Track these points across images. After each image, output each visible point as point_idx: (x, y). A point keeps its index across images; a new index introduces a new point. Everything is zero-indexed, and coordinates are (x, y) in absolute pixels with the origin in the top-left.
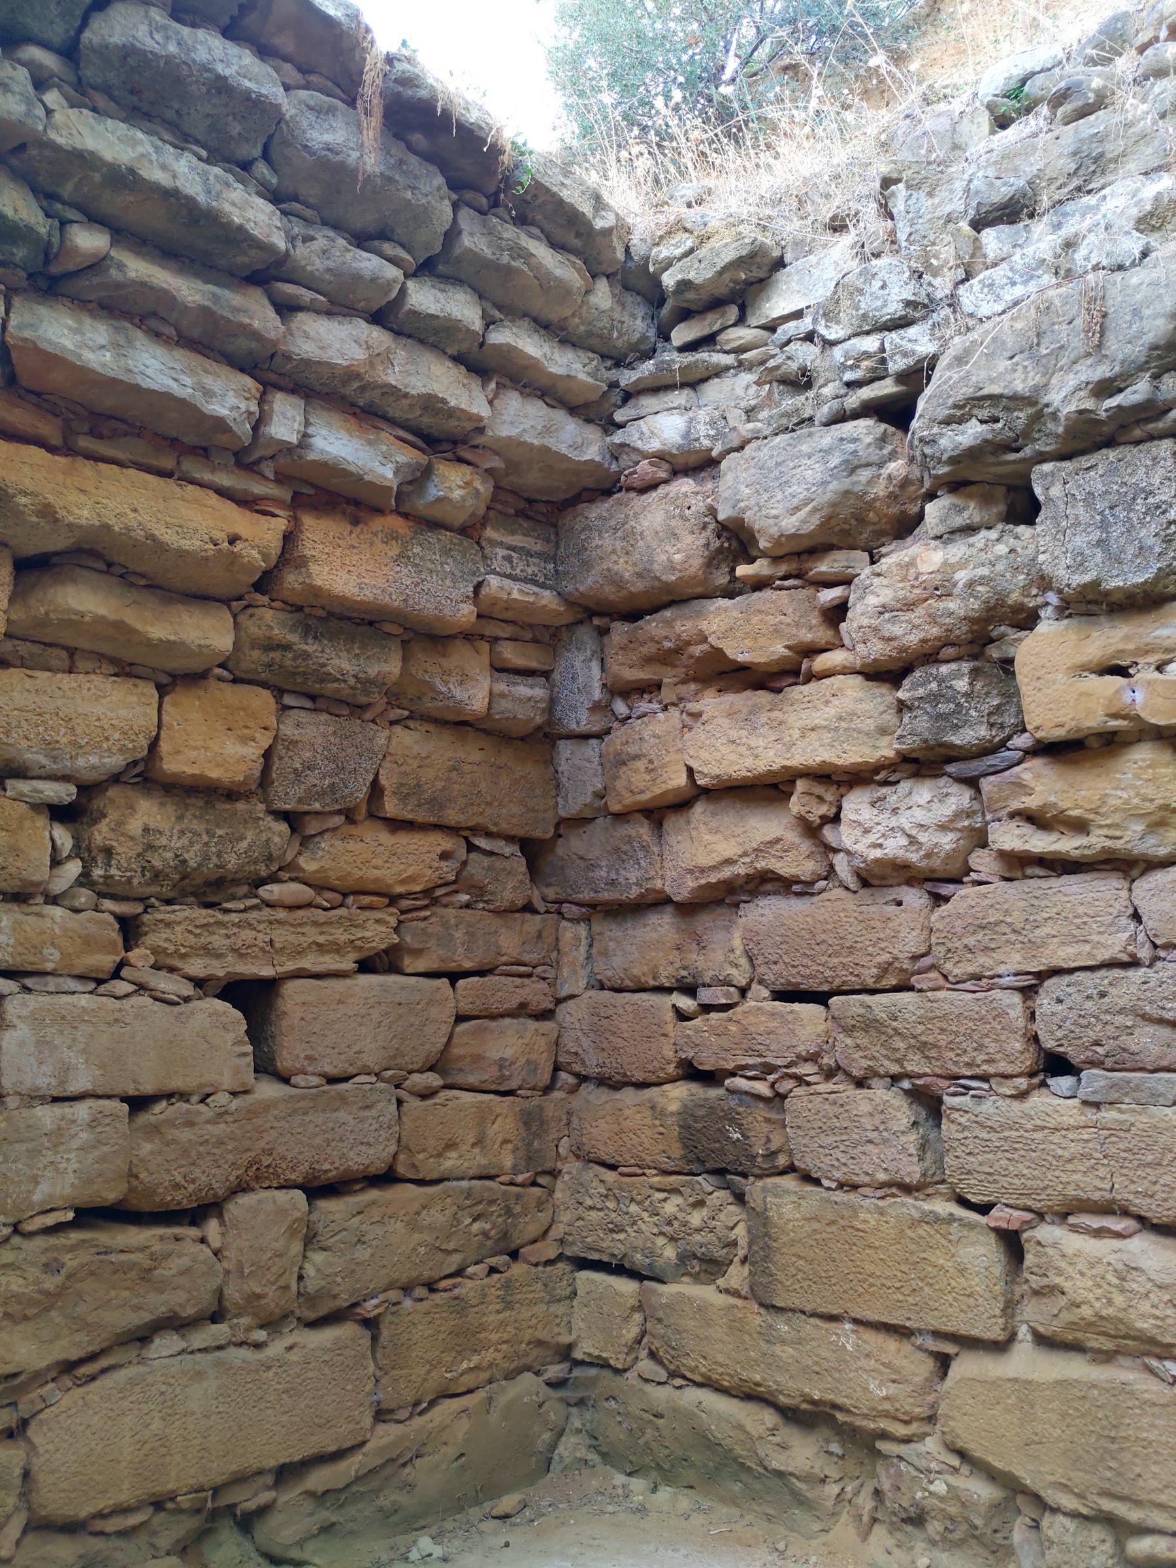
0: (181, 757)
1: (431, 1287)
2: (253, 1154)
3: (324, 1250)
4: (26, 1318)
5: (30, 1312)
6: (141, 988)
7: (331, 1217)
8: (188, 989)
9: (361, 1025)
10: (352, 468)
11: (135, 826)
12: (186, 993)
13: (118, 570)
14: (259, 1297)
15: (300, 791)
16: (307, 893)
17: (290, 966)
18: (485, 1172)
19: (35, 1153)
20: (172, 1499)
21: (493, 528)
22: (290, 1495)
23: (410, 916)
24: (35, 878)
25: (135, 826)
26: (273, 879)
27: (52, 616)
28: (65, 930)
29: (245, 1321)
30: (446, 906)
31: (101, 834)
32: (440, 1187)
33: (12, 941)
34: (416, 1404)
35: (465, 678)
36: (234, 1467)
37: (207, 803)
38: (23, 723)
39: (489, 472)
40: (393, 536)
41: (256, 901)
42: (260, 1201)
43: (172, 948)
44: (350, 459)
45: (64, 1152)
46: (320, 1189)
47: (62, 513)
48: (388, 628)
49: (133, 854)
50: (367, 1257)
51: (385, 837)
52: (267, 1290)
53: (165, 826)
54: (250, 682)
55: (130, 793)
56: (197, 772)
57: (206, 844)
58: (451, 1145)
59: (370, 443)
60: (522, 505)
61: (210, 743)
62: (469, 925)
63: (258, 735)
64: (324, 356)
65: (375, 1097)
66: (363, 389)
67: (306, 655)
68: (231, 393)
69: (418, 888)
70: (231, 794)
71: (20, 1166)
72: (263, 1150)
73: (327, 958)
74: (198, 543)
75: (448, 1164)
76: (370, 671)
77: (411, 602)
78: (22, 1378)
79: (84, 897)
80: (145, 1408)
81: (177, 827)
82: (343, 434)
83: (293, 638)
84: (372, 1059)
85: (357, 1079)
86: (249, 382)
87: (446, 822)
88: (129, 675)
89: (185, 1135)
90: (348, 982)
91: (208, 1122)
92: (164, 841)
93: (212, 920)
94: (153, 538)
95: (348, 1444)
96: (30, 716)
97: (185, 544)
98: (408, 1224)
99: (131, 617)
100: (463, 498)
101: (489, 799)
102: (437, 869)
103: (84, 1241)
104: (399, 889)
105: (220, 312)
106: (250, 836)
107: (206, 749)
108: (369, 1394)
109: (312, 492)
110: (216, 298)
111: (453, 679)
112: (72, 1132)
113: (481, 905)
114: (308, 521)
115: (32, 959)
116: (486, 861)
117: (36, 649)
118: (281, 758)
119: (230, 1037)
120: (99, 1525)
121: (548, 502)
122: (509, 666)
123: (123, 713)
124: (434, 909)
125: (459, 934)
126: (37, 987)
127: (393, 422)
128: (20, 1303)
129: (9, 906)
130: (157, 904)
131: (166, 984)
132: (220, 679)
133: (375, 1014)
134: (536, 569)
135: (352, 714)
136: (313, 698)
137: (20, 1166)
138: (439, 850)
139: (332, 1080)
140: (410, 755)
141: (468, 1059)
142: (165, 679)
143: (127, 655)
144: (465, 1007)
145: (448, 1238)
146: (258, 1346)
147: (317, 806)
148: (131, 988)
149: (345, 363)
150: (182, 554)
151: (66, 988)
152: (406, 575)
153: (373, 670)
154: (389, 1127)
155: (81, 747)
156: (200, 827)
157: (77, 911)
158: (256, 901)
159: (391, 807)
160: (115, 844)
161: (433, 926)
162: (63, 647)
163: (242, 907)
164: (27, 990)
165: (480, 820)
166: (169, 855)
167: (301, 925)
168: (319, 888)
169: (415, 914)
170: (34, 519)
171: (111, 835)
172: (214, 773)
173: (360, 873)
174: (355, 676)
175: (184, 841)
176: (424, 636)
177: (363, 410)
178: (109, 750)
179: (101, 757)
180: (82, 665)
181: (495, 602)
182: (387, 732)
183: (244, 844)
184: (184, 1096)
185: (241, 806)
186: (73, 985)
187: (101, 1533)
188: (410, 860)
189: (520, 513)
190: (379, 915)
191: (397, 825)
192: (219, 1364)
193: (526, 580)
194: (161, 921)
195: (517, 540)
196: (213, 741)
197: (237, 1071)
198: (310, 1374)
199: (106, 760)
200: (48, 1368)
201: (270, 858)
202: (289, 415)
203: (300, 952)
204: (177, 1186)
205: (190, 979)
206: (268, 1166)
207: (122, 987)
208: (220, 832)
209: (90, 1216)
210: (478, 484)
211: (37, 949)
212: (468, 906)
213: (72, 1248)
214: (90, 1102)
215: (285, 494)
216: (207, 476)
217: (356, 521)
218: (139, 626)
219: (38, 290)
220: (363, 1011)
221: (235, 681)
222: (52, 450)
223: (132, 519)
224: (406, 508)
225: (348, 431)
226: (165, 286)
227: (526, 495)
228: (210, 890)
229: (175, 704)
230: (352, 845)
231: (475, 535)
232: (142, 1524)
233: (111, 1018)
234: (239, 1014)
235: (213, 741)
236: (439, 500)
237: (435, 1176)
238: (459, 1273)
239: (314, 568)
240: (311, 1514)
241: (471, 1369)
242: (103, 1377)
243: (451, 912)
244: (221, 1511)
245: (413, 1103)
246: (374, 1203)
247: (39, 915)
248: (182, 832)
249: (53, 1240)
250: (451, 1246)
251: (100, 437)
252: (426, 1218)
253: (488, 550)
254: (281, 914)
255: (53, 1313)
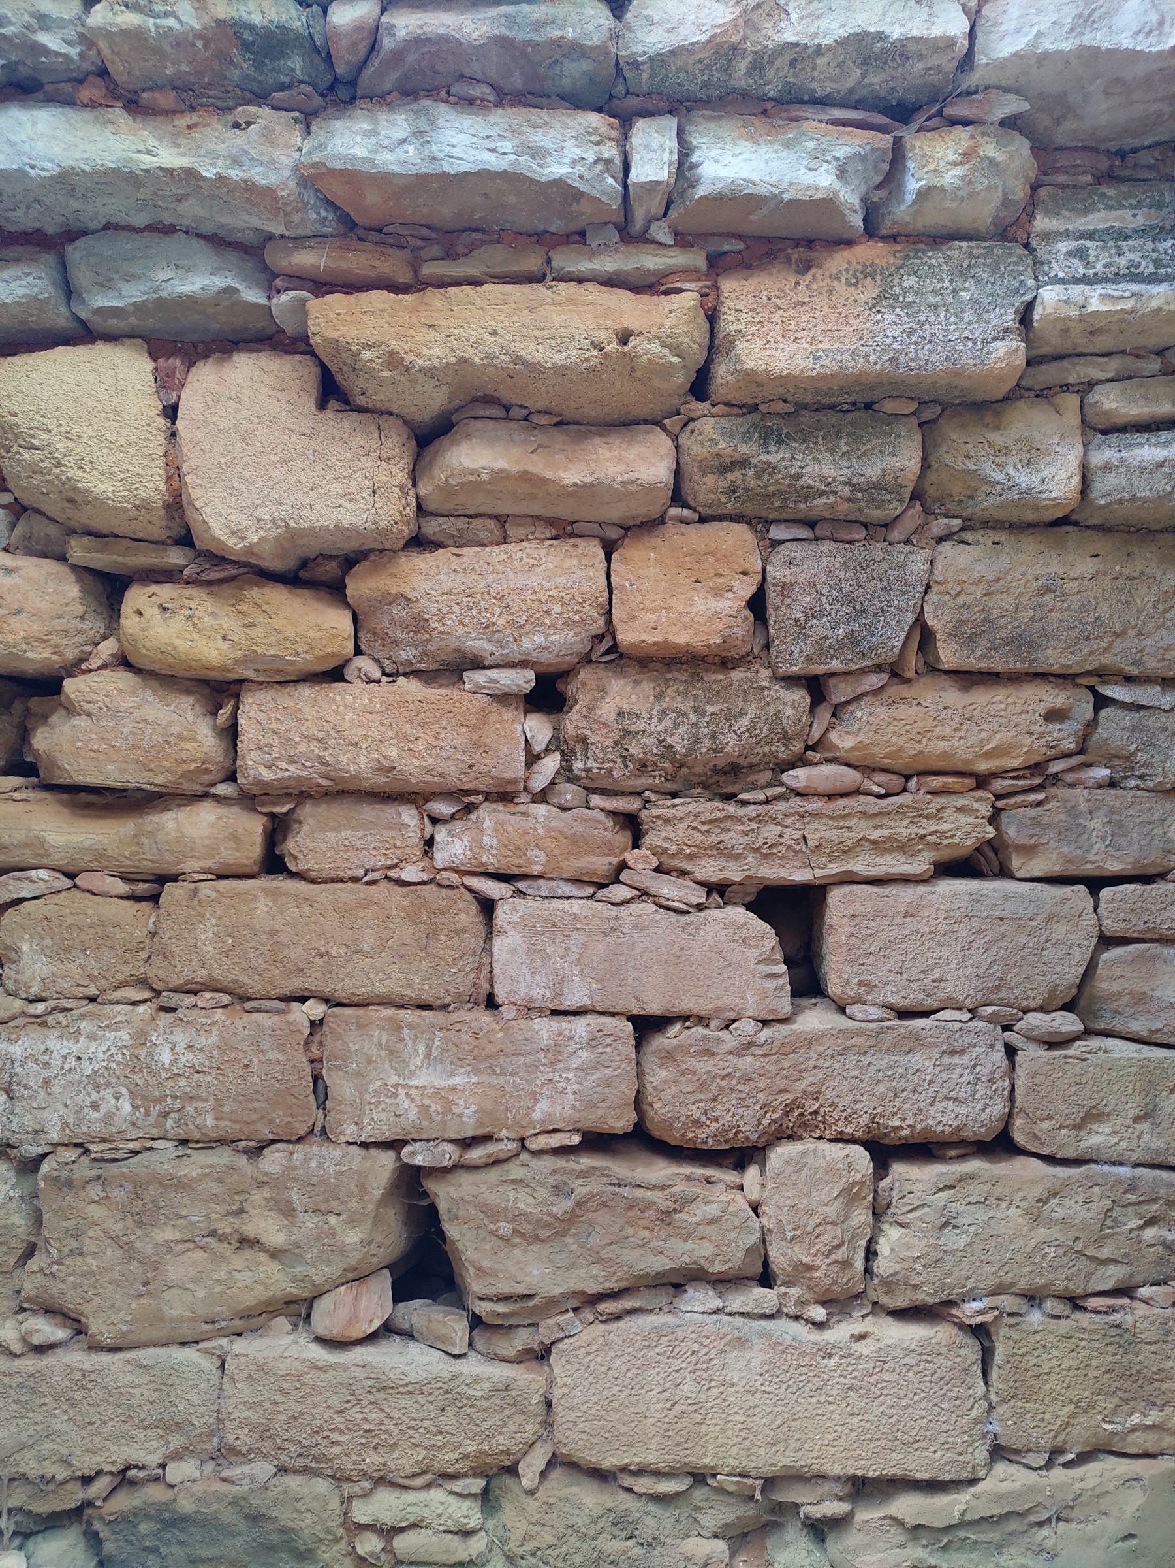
0: (637, 624)
1: (1075, 1302)
2: (791, 1096)
3: (901, 1225)
4: (538, 1239)
5: (544, 1233)
6: (643, 894)
7: (908, 1187)
8: (699, 896)
9: (941, 945)
10: (762, 190)
11: (607, 710)
12: (695, 900)
13: (516, 412)
14: (809, 1268)
15: (804, 648)
16: (851, 777)
17: (833, 869)
18: (1160, 1160)
19: (533, 1068)
20: (714, 1476)
21: (1048, 213)
22: (865, 1515)
23: (1012, 801)
24: (508, 775)
25: (607, 710)
26: (799, 761)
27: (452, 482)
28: (548, 830)
29: (795, 1292)
30: (1073, 786)
31: (573, 722)
32: (1083, 1169)
33: (495, 843)
34: (1056, 1452)
35: (1033, 454)
36: (786, 1461)
37: (692, 675)
38: (456, 608)
39: (1011, 123)
40: (868, 272)
41: (781, 789)
42: (804, 1153)
43: (673, 848)
44: (755, 177)
45: (562, 1070)
46: (885, 1151)
47: (409, 358)
48: (889, 406)
49: (609, 742)
50: (961, 1245)
51: (953, 696)
52: (818, 1262)
53: (642, 708)
54: (721, 518)
55: (602, 673)
56: (660, 639)
57: (695, 725)
58: (1093, 1116)
59: (787, 145)
60: (1104, 164)
61: (673, 602)
62: (1112, 811)
63: (735, 583)
64: (675, 40)
65: (967, 1040)
66: (757, 67)
67: (771, 469)
68: (569, 143)
69: (1015, 763)
70: (723, 660)
71: (518, 1080)
72: (804, 1092)
73: (888, 858)
74: (575, 353)
75: (1095, 1140)
76: (868, 472)
77: (903, 360)
78: (536, 1301)
79: (569, 793)
80: (676, 1364)
81: (657, 708)
82: (745, 146)
83: (746, 449)
84: (960, 987)
85: (939, 1015)
86: (594, 119)
87: (1045, 668)
88: (572, 535)
89: (704, 1065)
90: (922, 889)
91: (731, 1053)
92: (641, 725)
93: (720, 815)
94: (517, 360)
95: (947, 1477)
96: (460, 598)
97: (561, 358)
98: (1027, 1212)
99: (538, 466)
100: (967, 180)
101: (1118, 627)
102: (1041, 735)
103: (595, 1168)
104: (983, 766)
105: (520, 36)
106: (752, 710)
107: (668, 609)
108: (976, 1421)
109: (740, 246)
110: (510, 20)
111: (1011, 460)
112: (570, 1049)
113: (1133, 783)
114: (729, 286)
115: (518, 861)
116: (1129, 718)
117: (462, 523)
118: (777, 609)
119: (752, 954)
120: (628, 1481)
121: (1157, 144)
122: (1120, 421)
123: (561, 580)
124: (1053, 791)
125: (1095, 824)
126: (529, 891)
127: (824, 102)
128: (530, 1223)
129: (494, 806)
130: (653, 797)
131: (670, 889)
132: (684, 521)
133: (963, 931)
134: (1136, 257)
135: (870, 537)
136: (811, 524)
137: (518, 1080)
138: (1042, 708)
139: (904, 1014)
140: (970, 576)
141: (1126, 999)
142: (613, 533)
143: (562, 510)
144: (1112, 926)
145: (1100, 1241)
146: (820, 1326)
147: (836, 665)
148: (628, 893)
149: (704, 38)
150: (562, 371)
151: (560, 893)
152: (892, 324)
153: (873, 471)
154: (991, 1081)
155: (521, 627)
156: (681, 703)
157: (565, 809)
158: (781, 789)
159: (948, 654)
160: (588, 733)
161: (1053, 814)
162: (490, 516)
163: (762, 797)
164: (522, 894)
165: (1107, 660)
166: (650, 741)
167: (845, 817)
168: (867, 769)
169: (1019, 799)
170: (387, 374)
171: (584, 723)
172: (681, 638)
173: (918, 747)
174: (847, 483)
175: (667, 723)
176: (946, 408)
177: (778, 101)
178: (553, 626)
179: (547, 636)
180: (512, 532)
181: (1064, 326)
182: (926, 554)
183: (745, 722)
184: (702, 1020)
185: (737, 675)
186: (568, 889)
187: (629, 1490)
188: (1006, 724)
189: (1111, 177)
190: (960, 801)
191: (967, 678)
192: (765, 1335)
193: (1116, 278)
194: (658, 817)
195: (1097, 220)
196: (682, 595)
197: (763, 995)
198: (886, 1376)
199: (551, 638)
200: (566, 1296)
201: (786, 738)
202: (655, 145)
203: (847, 851)
204: (697, 1123)
205: (701, 884)
206: (816, 1113)
207: (619, 892)
208: (711, 709)
209: (597, 1142)
210: (990, 149)
211: (521, 851)
212: (1112, 784)
213: (583, 1174)
214: (589, 1019)
215: (697, 259)
216: (584, 266)
217: (805, 267)
218: (549, 474)
219: (335, 104)
220: (943, 927)
221: (702, 520)
222: (395, 288)
223: (491, 345)
224: (886, 228)
225: (752, 139)
226: (442, 31)
227: (1113, 146)
228: (724, 780)
229: (625, 561)
230: (902, 711)
231: (1021, 235)
232: (677, 1494)
233: (606, 927)
234: (766, 927)
235: (682, 595)
236: (923, 194)
237: (1070, 1154)
238: (1125, 1291)
239: (741, 347)
240: (902, 1546)
241: (1148, 1427)
242: (627, 1319)
243: (1080, 795)
244: (768, 1507)
245: (1031, 1055)
246: (972, 1177)
247: (525, 814)
248: (663, 713)
249: (561, 1162)
250: (1105, 1253)
251: (457, 257)
252: (1057, 1209)
253: (1042, 253)
254: (814, 805)
255: (568, 1240)
